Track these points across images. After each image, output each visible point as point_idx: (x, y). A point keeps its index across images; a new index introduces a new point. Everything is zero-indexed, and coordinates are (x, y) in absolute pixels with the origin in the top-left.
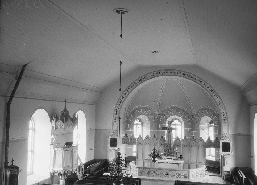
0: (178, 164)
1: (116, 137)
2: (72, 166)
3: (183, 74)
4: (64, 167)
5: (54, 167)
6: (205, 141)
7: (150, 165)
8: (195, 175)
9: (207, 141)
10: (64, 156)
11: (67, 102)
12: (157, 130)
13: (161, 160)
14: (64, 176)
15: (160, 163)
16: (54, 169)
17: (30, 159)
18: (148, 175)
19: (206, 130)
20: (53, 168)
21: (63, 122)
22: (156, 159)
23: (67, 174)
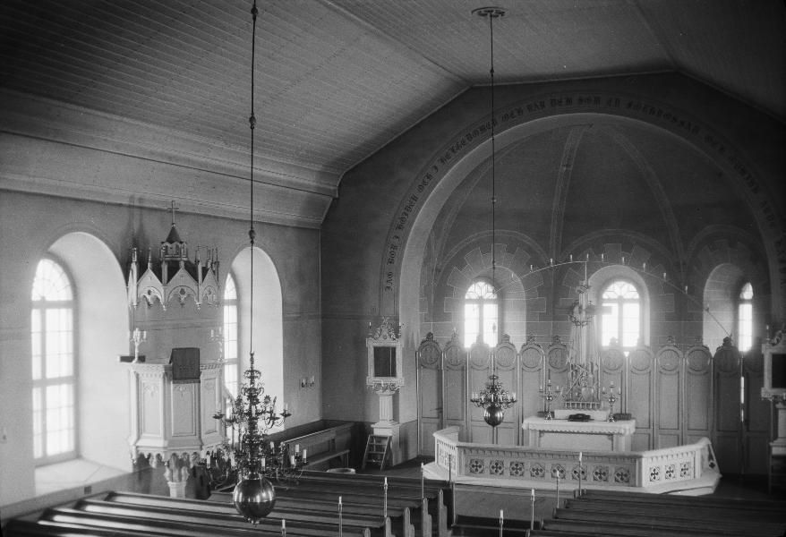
0: (610, 435)
1: (393, 344)
2: (200, 437)
3: (630, 105)
4: (171, 441)
5: (139, 438)
6: (713, 352)
7: (514, 440)
8: (678, 469)
9: (720, 351)
10: (463, 395)
11: (481, 309)
12: (554, 320)
13: (552, 422)
14: (180, 471)
15: (548, 432)
16: (138, 444)
17: (40, 414)
18: (491, 473)
19: (725, 319)
20: (134, 437)
21: (160, 278)
22: (499, 415)
23: (188, 464)
